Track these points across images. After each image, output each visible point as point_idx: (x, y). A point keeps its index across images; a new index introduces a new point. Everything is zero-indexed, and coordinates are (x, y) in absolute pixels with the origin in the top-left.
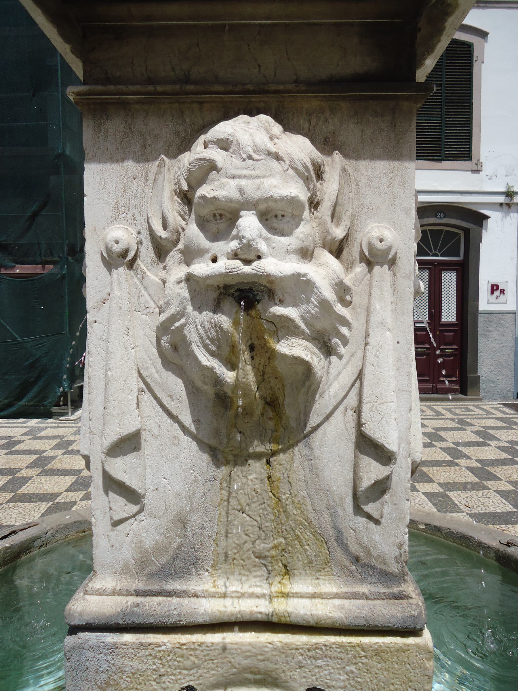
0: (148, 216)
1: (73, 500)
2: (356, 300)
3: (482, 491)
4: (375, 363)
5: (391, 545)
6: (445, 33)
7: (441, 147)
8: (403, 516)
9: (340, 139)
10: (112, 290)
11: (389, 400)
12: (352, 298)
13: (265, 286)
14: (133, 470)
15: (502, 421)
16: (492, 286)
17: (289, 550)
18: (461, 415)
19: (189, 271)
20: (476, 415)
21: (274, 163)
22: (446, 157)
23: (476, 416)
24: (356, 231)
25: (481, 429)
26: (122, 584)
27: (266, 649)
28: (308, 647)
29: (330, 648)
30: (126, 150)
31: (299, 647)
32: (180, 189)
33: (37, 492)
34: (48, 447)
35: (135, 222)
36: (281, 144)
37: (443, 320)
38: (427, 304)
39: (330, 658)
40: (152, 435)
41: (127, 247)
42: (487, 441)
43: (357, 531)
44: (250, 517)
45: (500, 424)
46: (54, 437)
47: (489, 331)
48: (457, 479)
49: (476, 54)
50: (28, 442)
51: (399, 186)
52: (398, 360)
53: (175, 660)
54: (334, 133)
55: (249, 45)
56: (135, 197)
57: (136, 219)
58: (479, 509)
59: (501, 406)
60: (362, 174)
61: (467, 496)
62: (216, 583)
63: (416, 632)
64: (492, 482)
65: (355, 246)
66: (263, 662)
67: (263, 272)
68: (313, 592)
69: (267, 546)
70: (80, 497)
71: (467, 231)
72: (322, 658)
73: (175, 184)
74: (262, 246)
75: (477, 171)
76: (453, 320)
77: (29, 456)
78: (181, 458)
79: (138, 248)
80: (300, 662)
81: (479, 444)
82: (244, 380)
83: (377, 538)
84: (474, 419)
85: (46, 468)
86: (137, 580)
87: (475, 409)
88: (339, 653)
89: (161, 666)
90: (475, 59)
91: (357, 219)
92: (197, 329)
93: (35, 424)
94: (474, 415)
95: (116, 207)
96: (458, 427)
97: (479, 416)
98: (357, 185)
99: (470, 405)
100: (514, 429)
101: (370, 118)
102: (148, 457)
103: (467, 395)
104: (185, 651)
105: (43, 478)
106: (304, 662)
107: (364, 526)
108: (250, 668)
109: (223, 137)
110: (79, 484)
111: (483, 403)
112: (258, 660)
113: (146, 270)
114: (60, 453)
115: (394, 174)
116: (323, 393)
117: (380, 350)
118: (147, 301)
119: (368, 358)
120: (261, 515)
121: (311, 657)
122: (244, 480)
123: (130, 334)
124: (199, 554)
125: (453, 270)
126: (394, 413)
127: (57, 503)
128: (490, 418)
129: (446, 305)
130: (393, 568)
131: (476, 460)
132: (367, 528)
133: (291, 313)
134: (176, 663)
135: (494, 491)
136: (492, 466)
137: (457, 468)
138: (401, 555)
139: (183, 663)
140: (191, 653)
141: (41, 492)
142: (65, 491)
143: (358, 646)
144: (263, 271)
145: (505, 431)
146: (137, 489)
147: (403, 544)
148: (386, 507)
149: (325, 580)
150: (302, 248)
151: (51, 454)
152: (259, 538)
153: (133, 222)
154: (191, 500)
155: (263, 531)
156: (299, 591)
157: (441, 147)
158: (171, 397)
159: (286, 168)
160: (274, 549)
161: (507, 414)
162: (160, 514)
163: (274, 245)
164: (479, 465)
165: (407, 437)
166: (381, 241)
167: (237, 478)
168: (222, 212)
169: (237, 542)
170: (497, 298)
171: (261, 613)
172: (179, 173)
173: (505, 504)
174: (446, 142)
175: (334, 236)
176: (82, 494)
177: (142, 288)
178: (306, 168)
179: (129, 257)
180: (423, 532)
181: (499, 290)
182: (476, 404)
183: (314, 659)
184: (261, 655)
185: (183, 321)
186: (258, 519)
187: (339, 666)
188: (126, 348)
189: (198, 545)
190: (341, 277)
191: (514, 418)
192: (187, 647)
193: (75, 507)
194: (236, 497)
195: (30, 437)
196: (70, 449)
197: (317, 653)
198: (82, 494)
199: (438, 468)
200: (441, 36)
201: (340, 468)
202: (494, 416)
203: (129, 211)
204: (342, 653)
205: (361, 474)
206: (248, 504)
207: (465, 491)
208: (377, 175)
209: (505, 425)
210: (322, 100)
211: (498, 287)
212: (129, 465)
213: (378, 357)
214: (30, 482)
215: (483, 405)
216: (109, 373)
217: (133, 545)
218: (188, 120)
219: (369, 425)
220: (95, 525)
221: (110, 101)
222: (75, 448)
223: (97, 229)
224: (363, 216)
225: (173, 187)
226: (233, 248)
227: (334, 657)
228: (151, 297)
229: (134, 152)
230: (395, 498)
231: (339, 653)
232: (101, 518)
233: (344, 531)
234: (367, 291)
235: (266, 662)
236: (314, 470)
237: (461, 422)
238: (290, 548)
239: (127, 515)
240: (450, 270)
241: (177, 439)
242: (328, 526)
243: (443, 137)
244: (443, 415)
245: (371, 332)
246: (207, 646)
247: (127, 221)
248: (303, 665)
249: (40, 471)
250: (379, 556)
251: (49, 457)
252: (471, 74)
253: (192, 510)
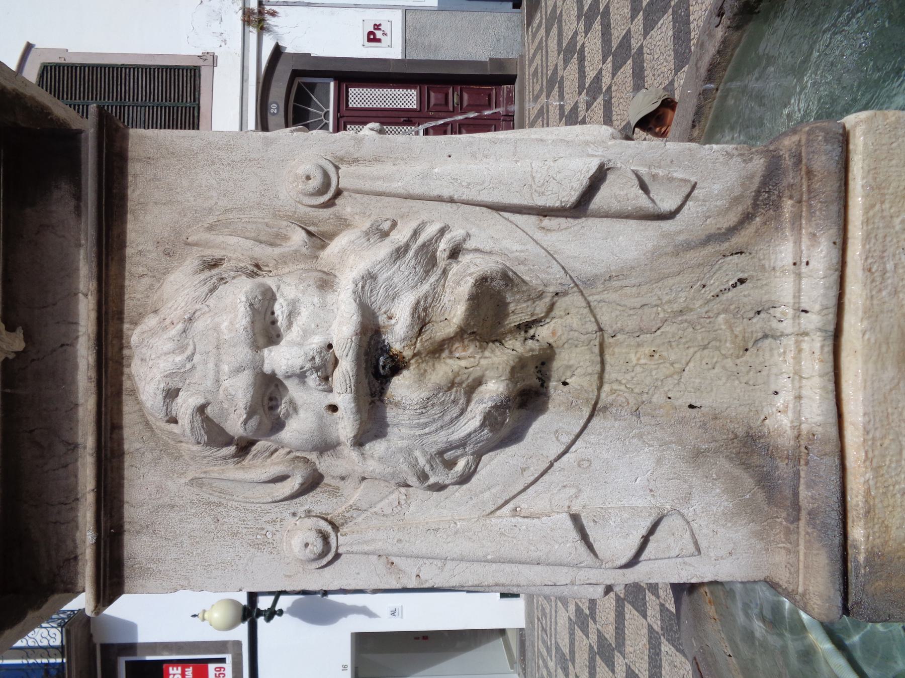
0: (271, 503)
1: (658, 608)
2: (390, 214)
3: (645, 55)
4: (478, 188)
5: (727, 168)
6: (21, 90)
7: (182, 108)
8: (687, 152)
9: (166, 235)
10: (373, 553)
11: (529, 169)
12: (388, 220)
13: (371, 338)
14: (625, 524)
15: (550, 29)
16: (369, 40)
17: (736, 308)
18: (542, 83)
19: (348, 444)
20: (542, 63)
21: (199, 325)
22: (194, 101)
23: (544, 63)
24: (295, 212)
25: (561, 56)
26: (783, 540)
27: (873, 341)
28: (868, 282)
29: (869, 251)
30: (178, 532)
31: (869, 294)
32: (234, 456)
33: (646, 658)
34: (586, 641)
35: (278, 520)
36: (172, 316)
37: (415, 107)
38: (393, 127)
39: (884, 251)
40: (576, 497)
41: (314, 531)
42: (578, 48)
43: (707, 214)
44: (689, 361)
45: (554, 31)
46: (572, 634)
47: (430, 45)
48: (628, 89)
49: (55, 60)
50: (577, 670)
51: (234, 154)
52: (474, 155)
53: (889, 467)
54: (158, 243)
55: (33, 360)
56: (244, 520)
57: (275, 518)
58: (669, 59)
59: (530, 30)
60: (216, 203)
61: (651, 74)
62: (781, 408)
63: (845, 138)
64: (633, 41)
65: (315, 214)
66: (890, 345)
67: (352, 341)
68: (792, 276)
69: (729, 338)
70: (654, 598)
71: (295, 74)
72: (884, 263)
73: (227, 463)
74: (316, 341)
75: (214, 59)
76: (415, 93)
77: (597, 669)
78: (609, 457)
79: (316, 516)
80: (890, 294)
81: (582, 59)
82: (500, 367)
83: (717, 187)
84: (547, 66)
85: (614, 646)
86: (777, 520)
87: (535, 65)
88: (877, 240)
89: (897, 487)
90: (62, 61)
91: (279, 211)
92: (430, 433)
93: (551, 660)
94: (542, 66)
95: (257, 546)
96: (559, 87)
97: (544, 59)
98: (230, 210)
99: (529, 71)
100: (561, 12)
101: (138, 192)
102: (607, 503)
103: (516, 76)
104: (876, 453)
105: (628, 649)
106: (889, 288)
107: (702, 205)
108: (898, 363)
109: (161, 396)
110: (636, 600)
111: (527, 54)
112: (887, 352)
113: (348, 504)
114: (594, 626)
115: (216, 161)
116: (519, 260)
117: (459, 181)
118: (390, 504)
119: (470, 198)
120: (687, 346)
121: (883, 279)
122: (638, 369)
123: (436, 527)
124: (741, 432)
125: (347, 92)
126: (546, 163)
127: (662, 629)
128: (546, 44)
129: (395, 102)
130: (758, 166)
131: (604, 63)
132: (704, 201)
133: (408, 303)
134: (893, 465)
135: (645, 38)
136: (611, 42)
137: (613, 88)
138: (741, 155)
139: (892, 456)
140: (879, 444)
141: (647, 652)
142: (646, 619)
143: (867, 213)
144: (349, 340)
145: (564, 24)
146: (652, 518)
147: (727, 152)
148: (675, 175)
149: (776, 258)
150: (318, 287)
151: (594, 637)
152: (718, 349)
153: (278, 524)
154: (665, 443)
155: (709, 343)
156: (792, 294)
157: (182, 108)
158: (523, 470)
159: (206, 309)
160: (734, 329)
161: (541, 22)
162: (686, 486)
163: (313, 326)
164: (610, 59)
165: (579, 145)
166: (308, 178)
167: (635, 379)
168: (266, 399)
169: (724, 379)
170: (386, 34)
171: (822, 347)
172: (211, 458)
173: (662, 25)
174: (174, 101)
175: (301, 243)
176: (649, 597)
177: (372, 510)
178: (205, 281)
179: (328, 528)
180: (703, 131)
181: (375, 31)
182: (527, 63)
183: (885, 274)
184: (880, 347)
185: (418, 453)
186: (692, 350)
187: (895, 240)
188: (456, 533)
189: (728, 434)
190: (359, 234)
191: (546, 12)
192: (870, 450)
193: (667, 605)
194: (662, 380)
195: (571, 667)
196: (587, 612)
197: (877, 271)
198: (649, 597)
199: (614, 113)
200: (25, 96)
201: (621, 238)
202: (544, 39)
203: (263, 529)
204: (876, 235)
205: (630, 208)
206: (672, 364)
207: (644, 77)
208: (218, 183)
209: (556, 25)
210: (112, 259)
211: (370, 33)
212: (618, 529)
213: (469, 184)
214: (633, 667)
215: (529, 54)
216: (489, 557)
217: (729, 525)
218: (137, 445)
219: (564, 197)
220: (702, 577)
221: (108, 555)
222: (587, 604)
223: (289, 574)
224: (274, 203)
225: (231, 466)
226: (318, 382)
227: (884, 246)
228: (384, 498)
229: (181, 521)
230: (663, 163)
231: (877, 240)
232: (692, 569)
233: (707, 233)
234: (378, 198)
235: (891, 341)
236: (625, 273)
237: (551, 83)
238: (732, 307)
239: (688, 532)
240: (347, 96)
241: (582, 463)
242: (702, 254)
243: (168, 104)
244: (542, 107)
245: (435, 193)
246: (869, 421)
247: (277, 531)
248: (893, 290)
249: (619, 655)
250: (743, 184)
251: (598, 641)
252: (83, 67)
253: (680, 442)
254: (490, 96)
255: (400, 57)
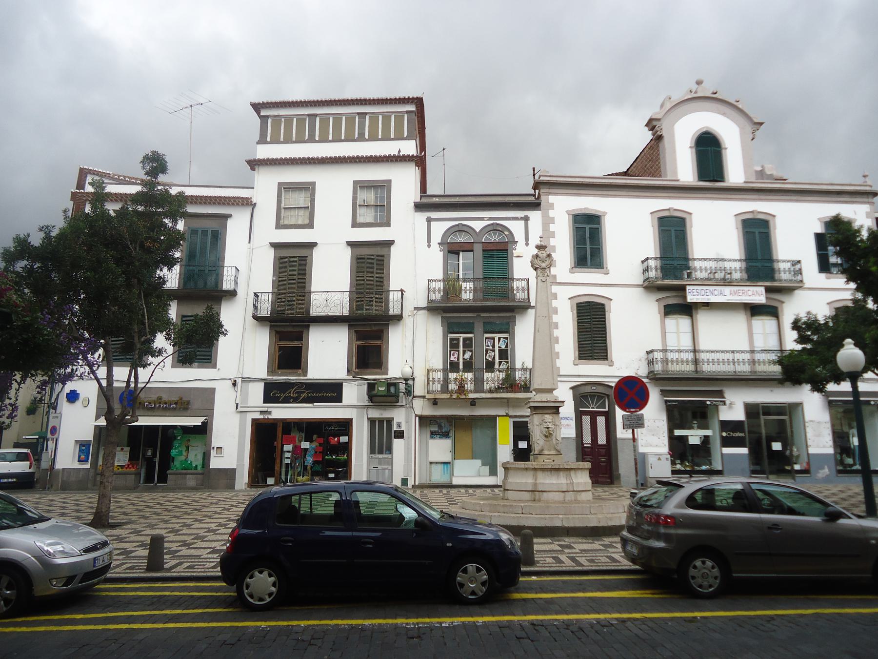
49: (606, 309)
252: (605, 318)
254: (606, 474)
255: (618, 437)
